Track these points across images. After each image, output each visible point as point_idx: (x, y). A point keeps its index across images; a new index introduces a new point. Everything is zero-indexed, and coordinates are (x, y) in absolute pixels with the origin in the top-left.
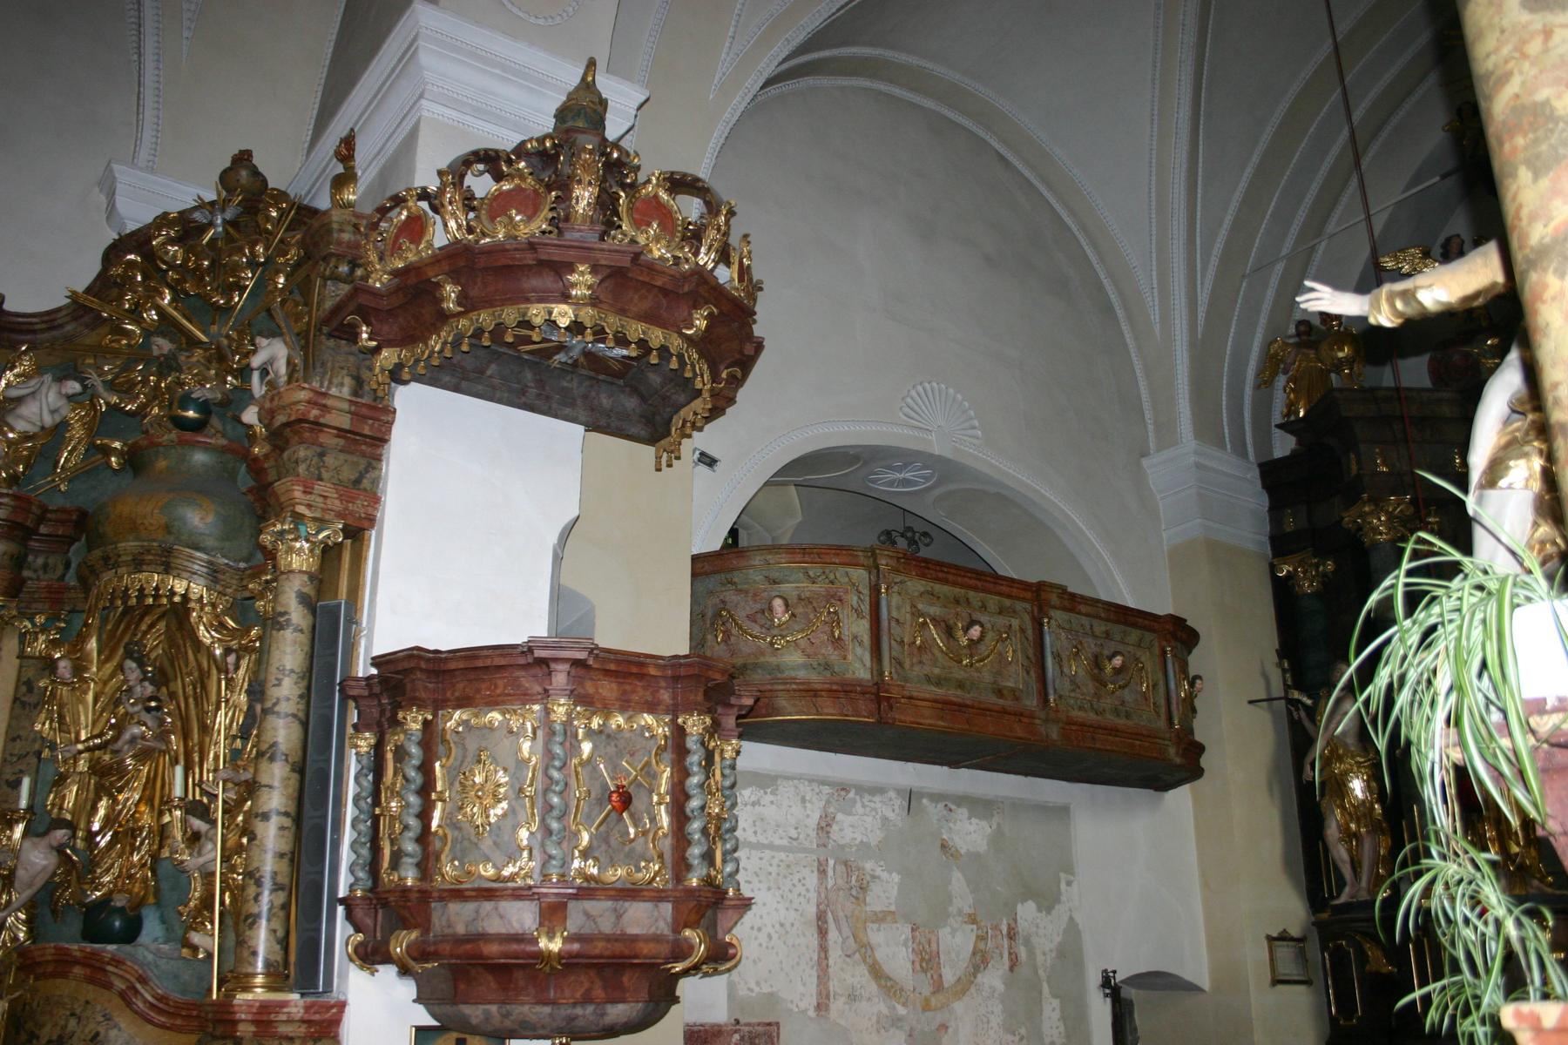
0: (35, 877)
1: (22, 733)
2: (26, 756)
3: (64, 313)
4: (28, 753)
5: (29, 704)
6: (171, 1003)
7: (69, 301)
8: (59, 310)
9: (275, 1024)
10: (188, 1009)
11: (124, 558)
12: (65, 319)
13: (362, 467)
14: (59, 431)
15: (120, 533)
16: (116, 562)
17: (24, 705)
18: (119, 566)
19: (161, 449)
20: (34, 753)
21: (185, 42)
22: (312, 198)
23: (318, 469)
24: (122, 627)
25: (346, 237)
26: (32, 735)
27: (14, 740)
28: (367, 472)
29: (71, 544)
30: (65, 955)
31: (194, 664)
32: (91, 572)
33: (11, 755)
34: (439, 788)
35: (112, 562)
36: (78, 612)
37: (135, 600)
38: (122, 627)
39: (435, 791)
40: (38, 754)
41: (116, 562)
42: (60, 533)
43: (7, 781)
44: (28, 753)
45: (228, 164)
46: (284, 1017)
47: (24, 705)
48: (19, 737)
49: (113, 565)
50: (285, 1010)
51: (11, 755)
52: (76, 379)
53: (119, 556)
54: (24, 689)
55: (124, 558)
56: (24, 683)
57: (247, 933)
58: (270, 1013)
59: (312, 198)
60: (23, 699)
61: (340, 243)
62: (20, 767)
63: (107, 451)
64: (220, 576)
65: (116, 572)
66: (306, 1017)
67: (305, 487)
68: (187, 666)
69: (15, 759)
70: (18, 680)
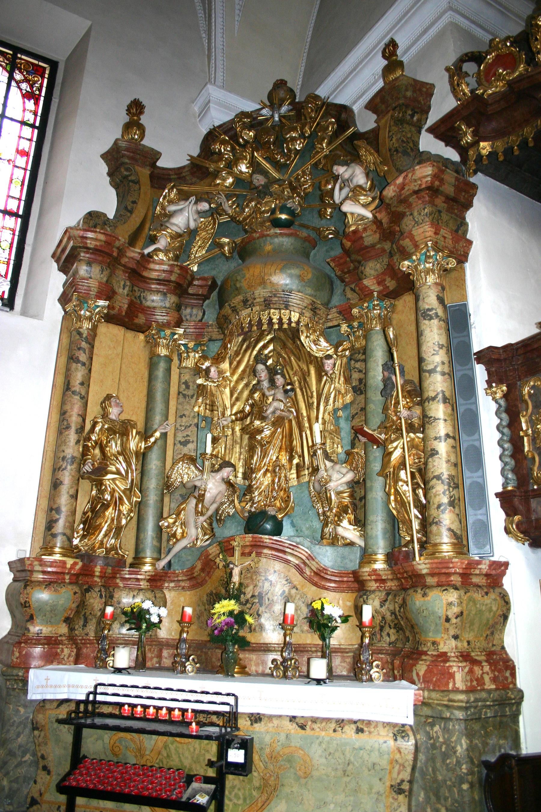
0: (216, 498)
1: (186, 413)
2: (189, 427)
3: (187, 169)
4: (191, 425)
5: (188, 396)
6: (329, 573)
7: (189, 162)
8: (183, 167)
9: (471, 577)
10: (341, 577)
11: (258, 300)
12: (187, 173)
13: (459, 223)
14: (192, 233)
15: (252, 286)
16: (252, 303)
17: (185, 396)
18: (254, 306)
19: (268, 238)
20: (195, 424)
21: (236, 23)
22: (335, 96)
23: (438, 221)
24: (244, 346)
25: (409, 94)
26: (192, 414)
27: (181, 417)
28: (462, 226)
29: (204, 301)
30: (260, 541)
31: (297, 368)
32: (233, 311)
33: (181, 426)
34: (524, 428)
35: (249, 303)
36: (213, 340)
37: (266, 326)
38: (244, 346)
39: (522, 430)
40: (197, 425)
41: (252, 303)
42: (200, 293)
43: (180, 441)
44: (191, 425)
45: (270, 87)
46: (477, 572)
47: (185, 396)
48: (184, 415)
49: (250, 305)
50: (479, 567)
51: (181, 426)
52: (206, 201)
53: (255, 299)
54: (184, 386)
55: (258, 300)
56: (183, 383)
57: (441, 516)
58: (471, 569)
59: (335, 96)
60: (184, 392)
61: (405, 97)
62: (187, 433)
63: (221, 246)
64: (318, 312)
65: (252, 310)
66: (489, 572)
67: (436, 230)
68: (292, 369)
69: (183, 428)
70: (179, 382)
